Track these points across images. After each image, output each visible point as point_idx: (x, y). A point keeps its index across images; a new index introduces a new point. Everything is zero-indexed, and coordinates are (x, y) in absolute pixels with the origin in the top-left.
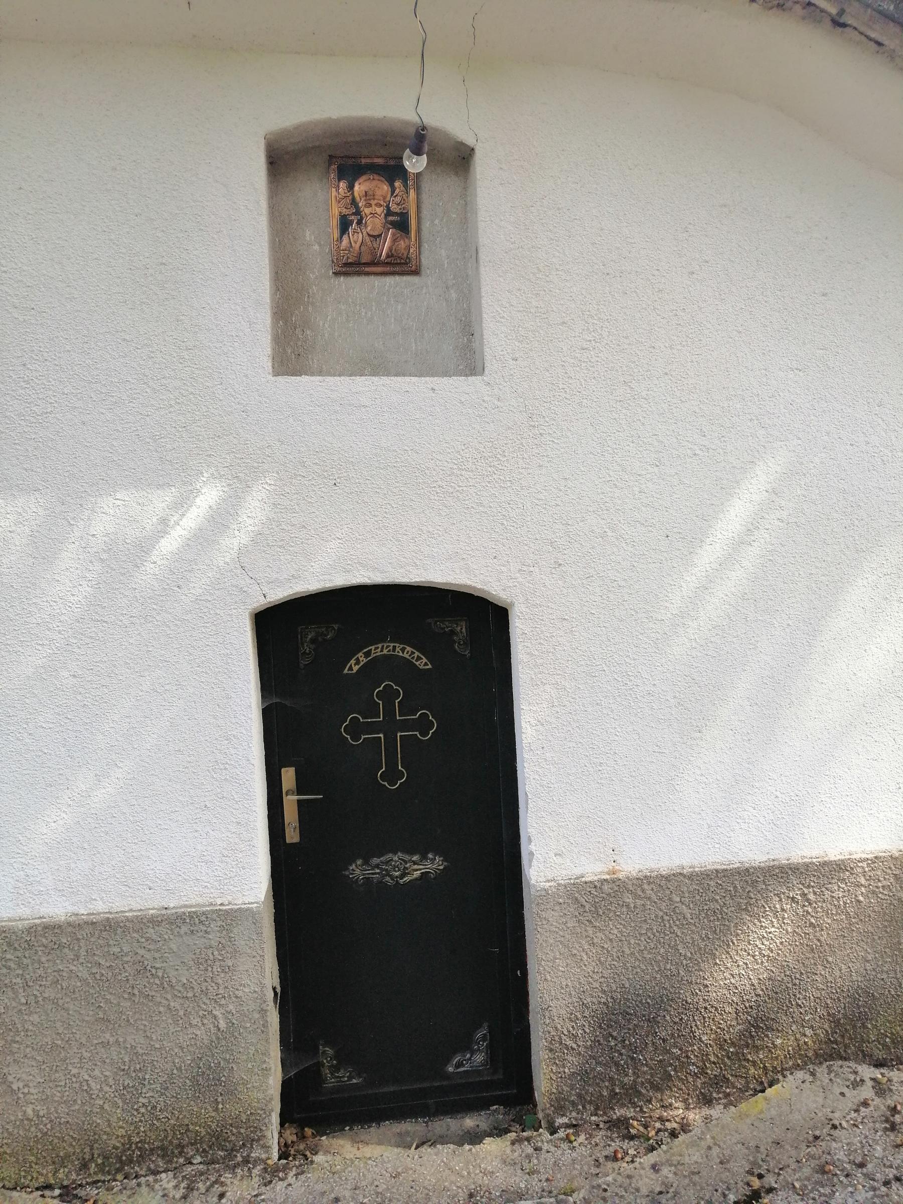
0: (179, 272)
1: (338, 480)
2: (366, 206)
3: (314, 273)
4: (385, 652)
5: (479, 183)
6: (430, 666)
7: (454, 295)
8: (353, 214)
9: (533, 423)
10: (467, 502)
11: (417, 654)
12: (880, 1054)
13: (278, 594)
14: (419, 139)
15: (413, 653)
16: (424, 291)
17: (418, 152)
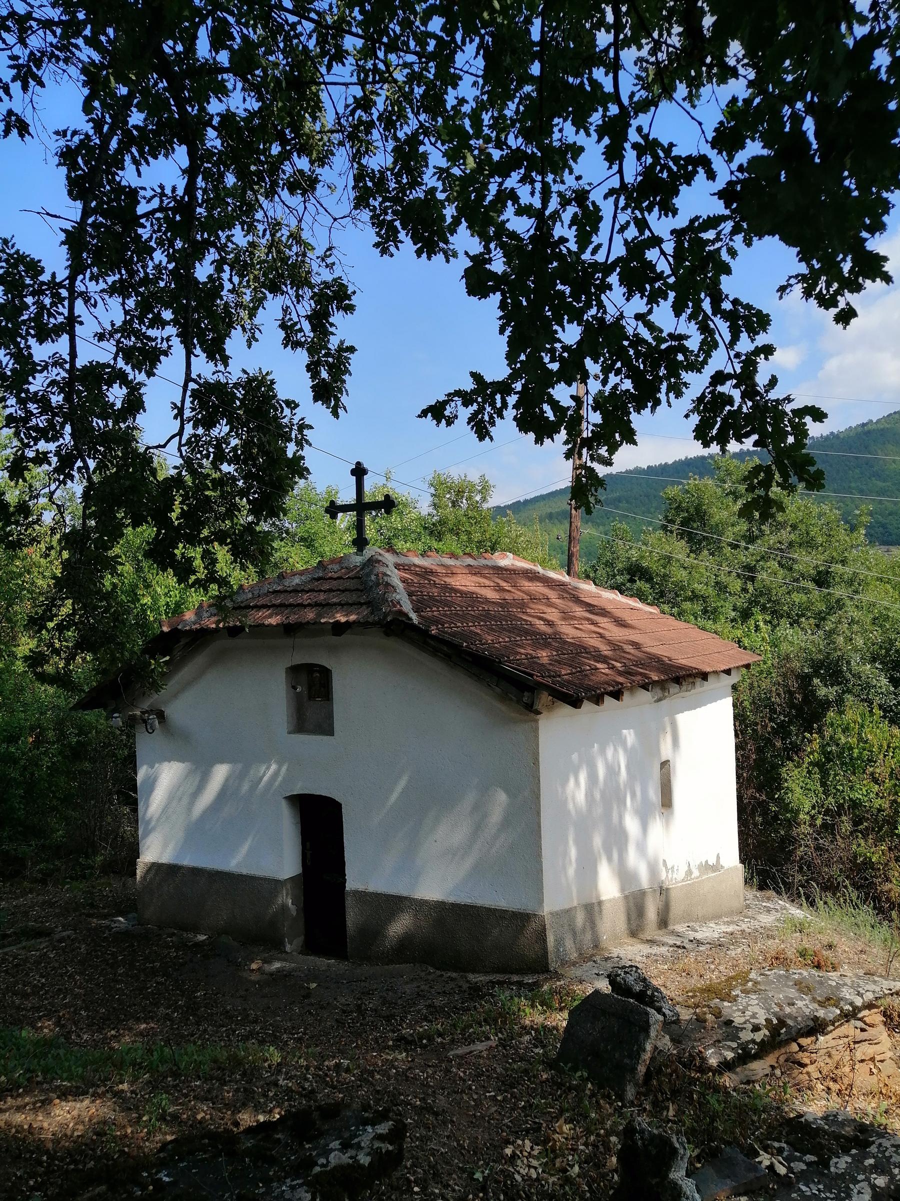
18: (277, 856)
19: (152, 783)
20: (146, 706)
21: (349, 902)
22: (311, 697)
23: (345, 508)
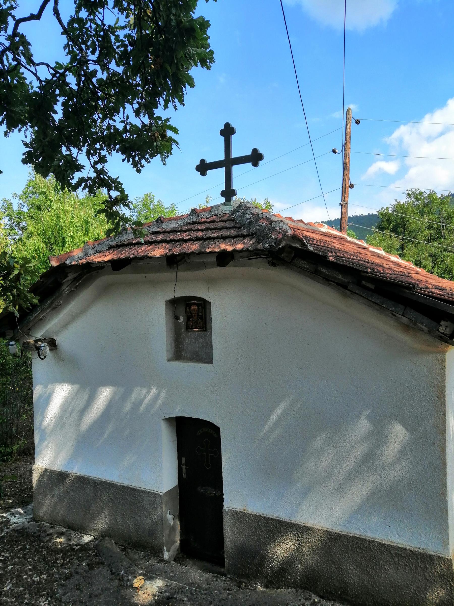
12: (321, 594)
18: (160, 474)
19: (48, 399)
20: (39, 334)
21: (227, 522)
22: (189, 328)
23: (215, 165)
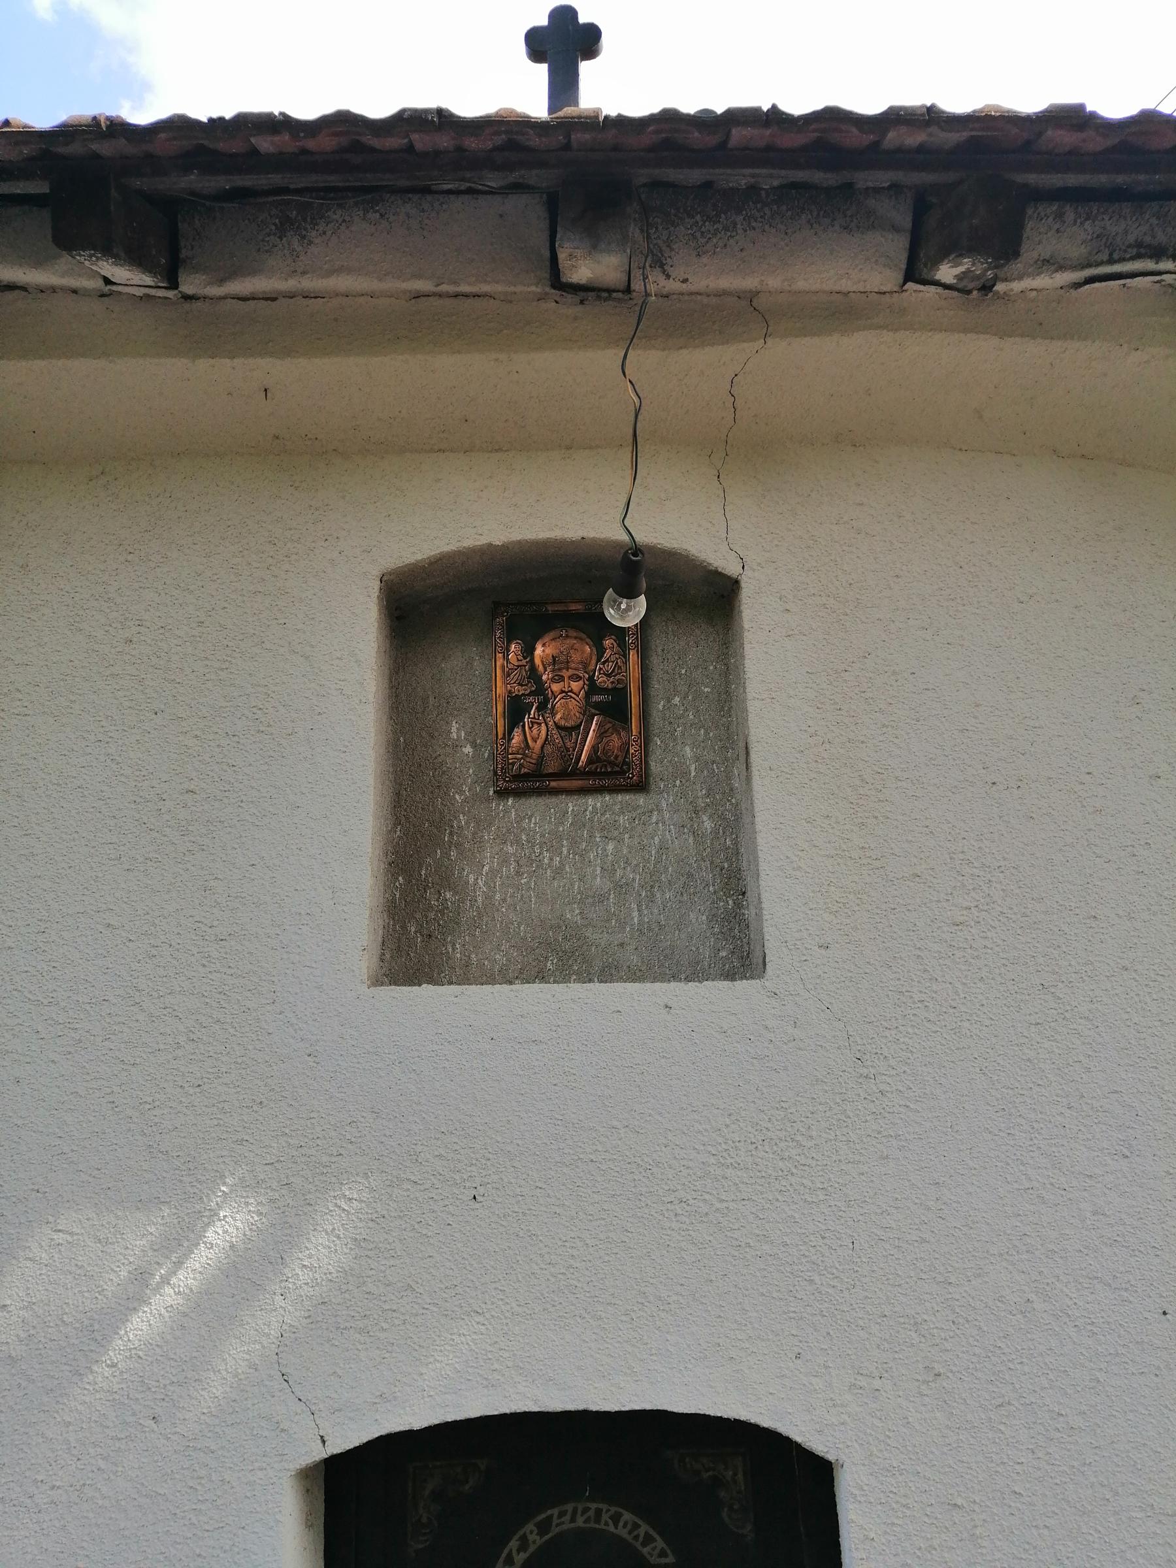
0: (217, 804)
1: (481, 1190)
2: (553, 680)
3: (461, 792)
4: (580, 1522)
5: (748, 637)
6: (670, 1559)
7: (708, 825)
8: (531, 694)
9: (865, 1071)
10: (736, 1234)
11: (644, 1528)
13: (348, 1437)
14: (629, 567)
15: (636, 1526)
16: (654, 819)
17: (630, 593)
